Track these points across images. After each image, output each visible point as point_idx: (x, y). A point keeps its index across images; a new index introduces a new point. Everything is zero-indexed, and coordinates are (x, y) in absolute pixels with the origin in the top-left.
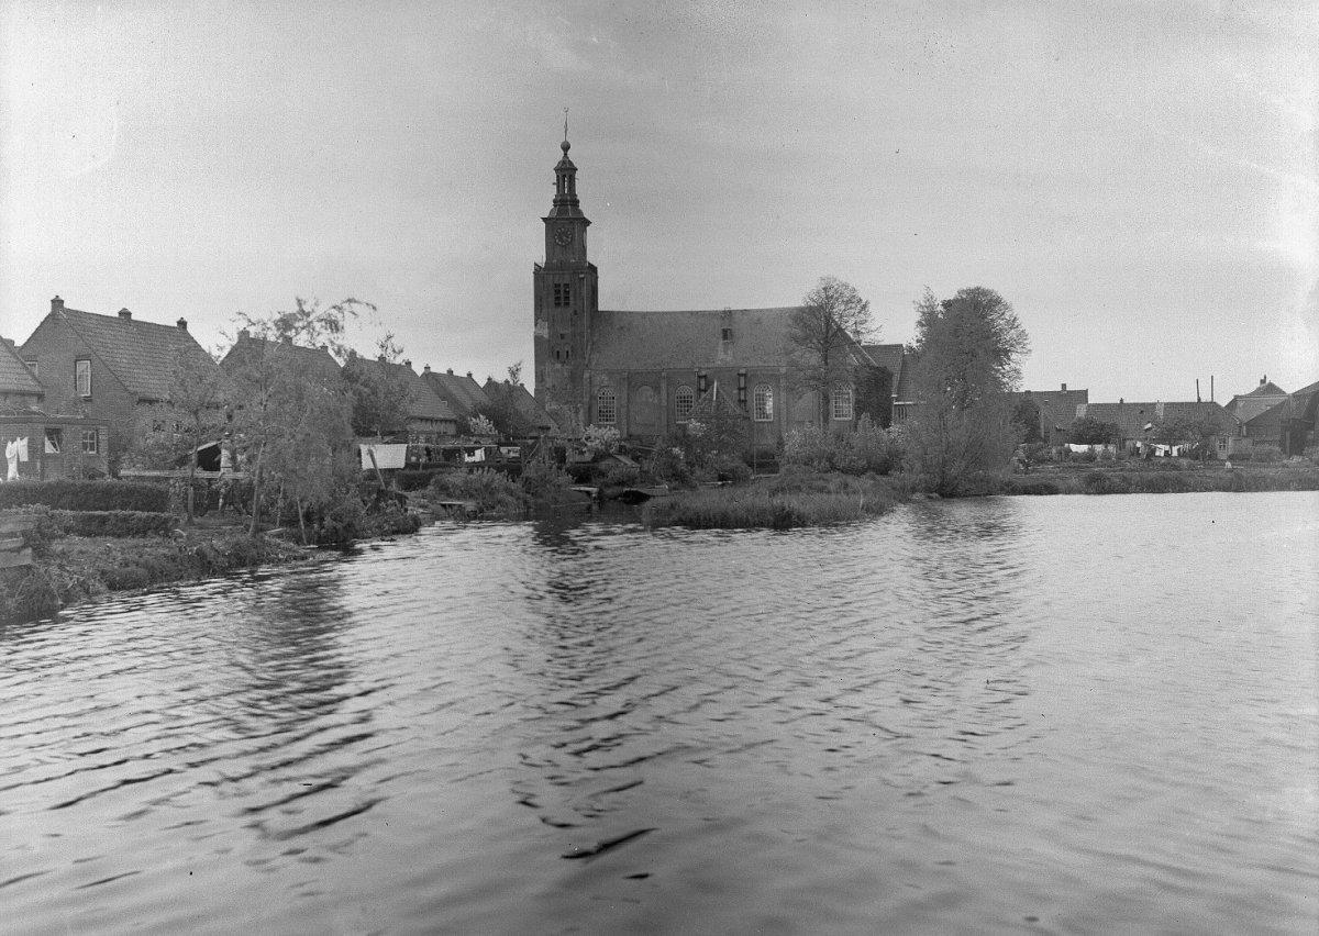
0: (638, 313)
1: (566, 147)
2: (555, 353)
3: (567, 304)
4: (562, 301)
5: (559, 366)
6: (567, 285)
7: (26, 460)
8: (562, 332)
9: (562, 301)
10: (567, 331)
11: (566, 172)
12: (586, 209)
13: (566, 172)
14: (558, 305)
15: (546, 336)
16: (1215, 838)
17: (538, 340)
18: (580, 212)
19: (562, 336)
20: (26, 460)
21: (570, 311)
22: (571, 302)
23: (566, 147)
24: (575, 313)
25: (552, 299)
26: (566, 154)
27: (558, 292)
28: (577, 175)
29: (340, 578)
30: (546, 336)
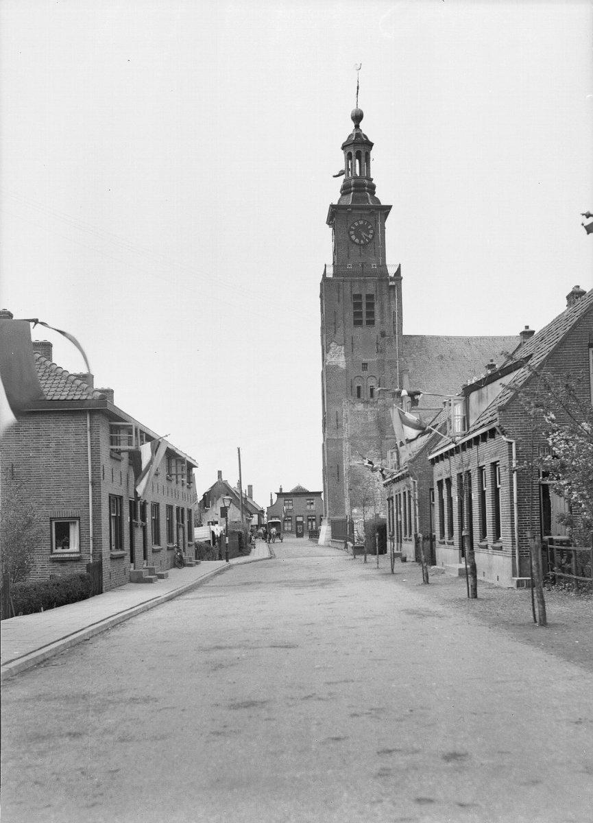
0: (455, 338)
1: (358, 118)
2: (355, 390)
3: (371, 323)
4: (364, 318)
5: (360, 407)
6: (370, 297)
7: (331, 276)
8: (364, 360)
9: (364, 318)
10: (372, 359)
11: (358, 148)
12: (383, 195)
13: (358, 148)
14: (358, 323)
15: (343, 365)
16: (486, 395)
17: (329, 373)
18: (377, 201)
19: (365, 366)
20: (331, 276)
21: (374, 332)
22: (377, 319)
23: (358, 118)
24: (383, 334)
25: (349, 316)
26: (357, 127)
27: (357, 306)
28: (373, 154)
29: (188, 509)
30: (343, 365)
